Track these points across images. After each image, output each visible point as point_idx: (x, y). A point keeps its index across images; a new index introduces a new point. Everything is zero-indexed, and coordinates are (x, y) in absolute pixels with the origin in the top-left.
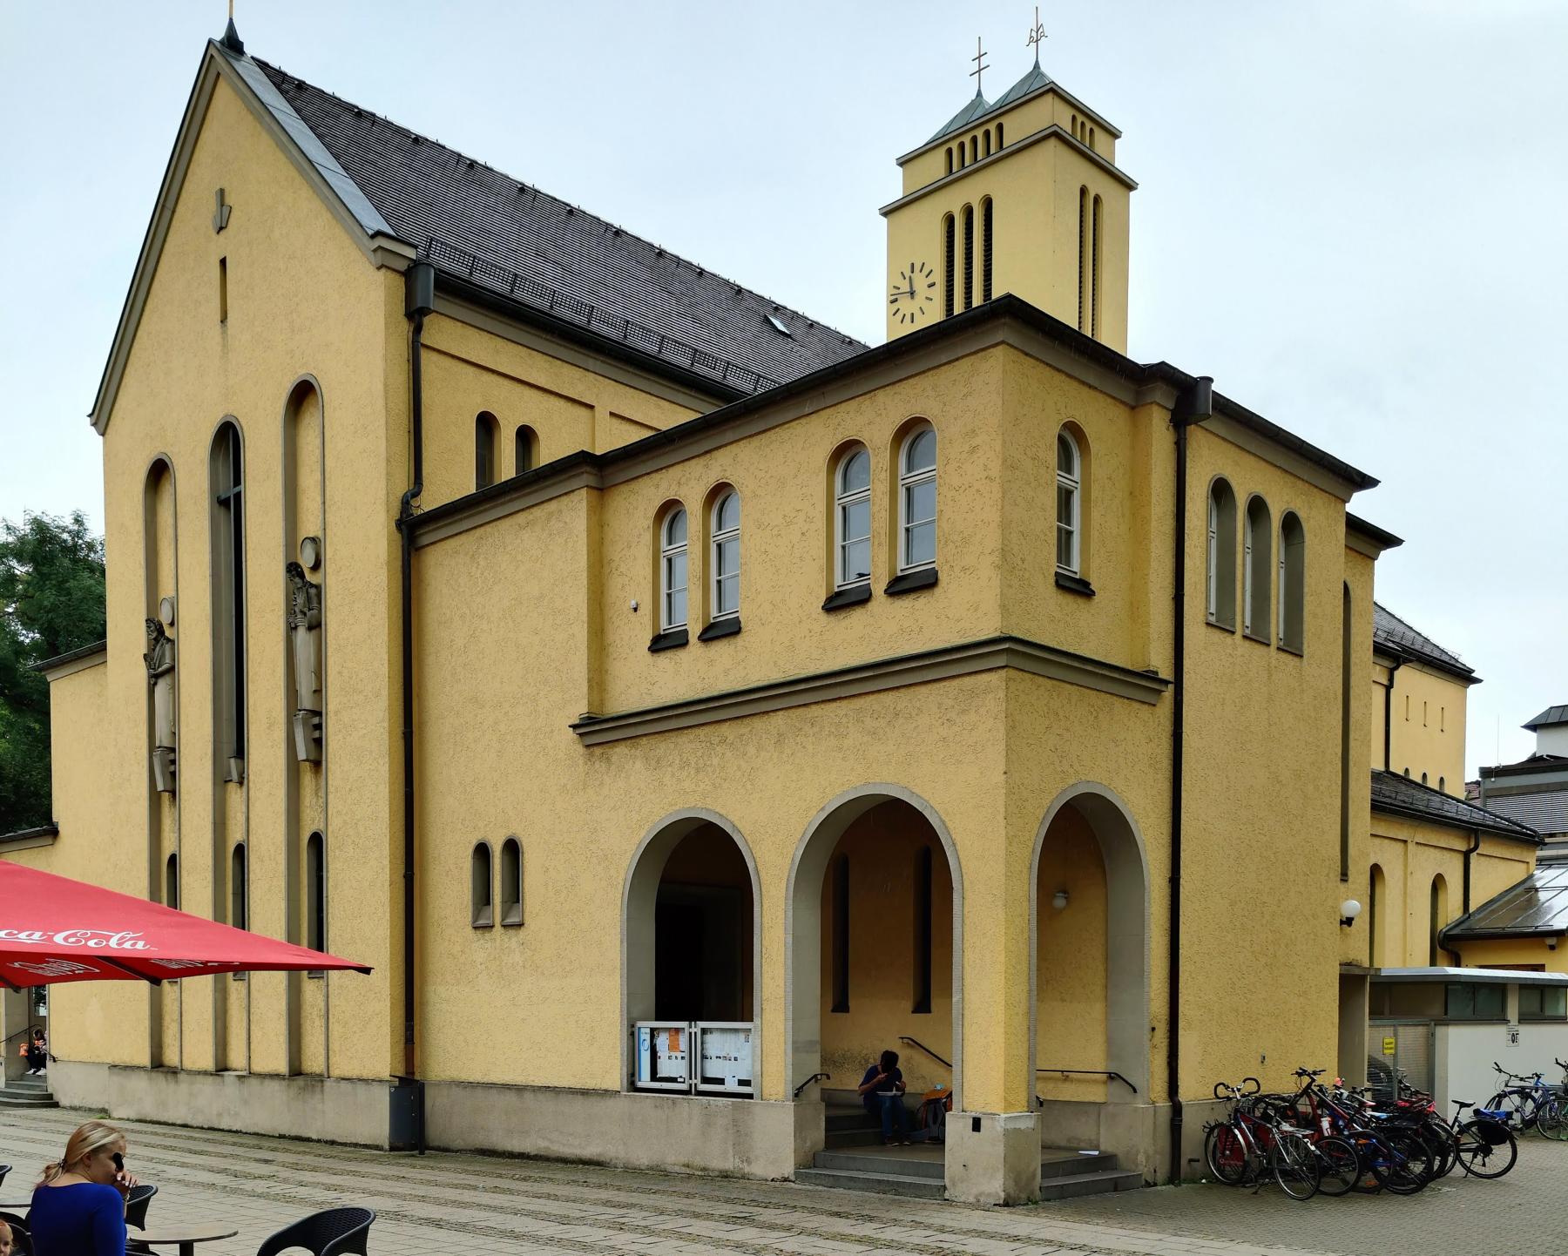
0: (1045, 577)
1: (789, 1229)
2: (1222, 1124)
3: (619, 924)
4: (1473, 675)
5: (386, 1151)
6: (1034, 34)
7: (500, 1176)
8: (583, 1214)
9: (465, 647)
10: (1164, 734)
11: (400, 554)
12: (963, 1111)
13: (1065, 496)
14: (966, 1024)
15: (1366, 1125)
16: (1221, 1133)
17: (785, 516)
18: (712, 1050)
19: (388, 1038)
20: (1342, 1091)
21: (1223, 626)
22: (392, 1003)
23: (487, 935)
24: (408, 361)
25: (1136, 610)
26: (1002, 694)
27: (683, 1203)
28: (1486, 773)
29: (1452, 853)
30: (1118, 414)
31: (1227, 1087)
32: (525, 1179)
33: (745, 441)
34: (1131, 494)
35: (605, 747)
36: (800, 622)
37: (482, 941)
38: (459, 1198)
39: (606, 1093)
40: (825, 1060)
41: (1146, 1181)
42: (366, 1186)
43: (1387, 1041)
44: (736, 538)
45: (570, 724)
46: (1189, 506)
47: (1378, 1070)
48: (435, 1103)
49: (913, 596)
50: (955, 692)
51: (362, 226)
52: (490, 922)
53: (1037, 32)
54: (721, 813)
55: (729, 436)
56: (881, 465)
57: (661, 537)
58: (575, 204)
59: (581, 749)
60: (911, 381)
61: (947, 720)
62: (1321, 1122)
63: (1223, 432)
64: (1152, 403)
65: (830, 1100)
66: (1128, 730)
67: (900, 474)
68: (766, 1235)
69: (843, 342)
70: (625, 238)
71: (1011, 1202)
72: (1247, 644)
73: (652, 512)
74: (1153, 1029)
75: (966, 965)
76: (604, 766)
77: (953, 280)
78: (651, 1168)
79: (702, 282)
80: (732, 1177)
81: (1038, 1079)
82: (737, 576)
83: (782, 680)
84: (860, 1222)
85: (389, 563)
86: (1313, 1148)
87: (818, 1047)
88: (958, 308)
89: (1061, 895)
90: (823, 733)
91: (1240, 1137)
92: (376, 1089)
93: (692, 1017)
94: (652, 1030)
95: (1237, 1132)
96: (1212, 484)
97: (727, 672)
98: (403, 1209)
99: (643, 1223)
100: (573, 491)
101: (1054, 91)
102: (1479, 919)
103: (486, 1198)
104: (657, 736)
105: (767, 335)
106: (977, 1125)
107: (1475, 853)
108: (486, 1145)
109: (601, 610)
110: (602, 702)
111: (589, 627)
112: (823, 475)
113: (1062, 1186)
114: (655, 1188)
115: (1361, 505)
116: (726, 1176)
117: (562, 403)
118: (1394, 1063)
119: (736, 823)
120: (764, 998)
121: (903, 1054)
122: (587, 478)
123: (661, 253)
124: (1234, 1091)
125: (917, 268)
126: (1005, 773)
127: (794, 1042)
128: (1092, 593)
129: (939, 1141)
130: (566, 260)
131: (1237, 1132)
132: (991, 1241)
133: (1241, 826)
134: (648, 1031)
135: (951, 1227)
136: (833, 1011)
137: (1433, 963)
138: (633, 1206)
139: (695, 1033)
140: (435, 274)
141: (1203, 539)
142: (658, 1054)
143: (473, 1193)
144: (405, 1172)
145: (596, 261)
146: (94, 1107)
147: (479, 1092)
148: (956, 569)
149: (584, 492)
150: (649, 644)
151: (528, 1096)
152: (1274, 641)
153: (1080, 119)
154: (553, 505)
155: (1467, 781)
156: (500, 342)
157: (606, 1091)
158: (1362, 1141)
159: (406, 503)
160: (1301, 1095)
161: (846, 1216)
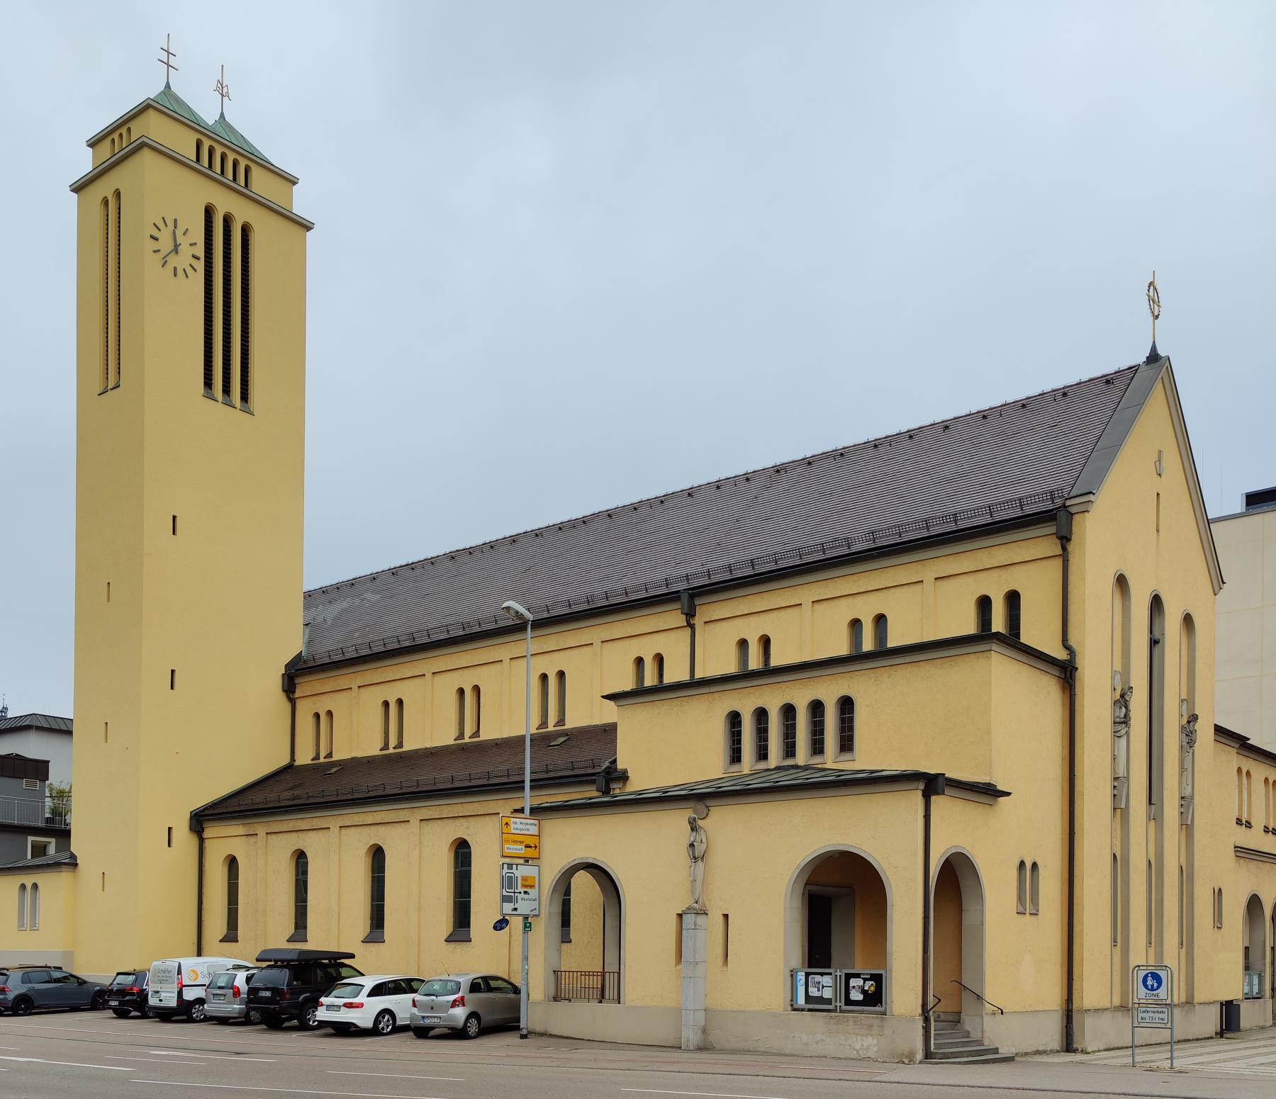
4: (1248, 742)
146: (1030, 1051)
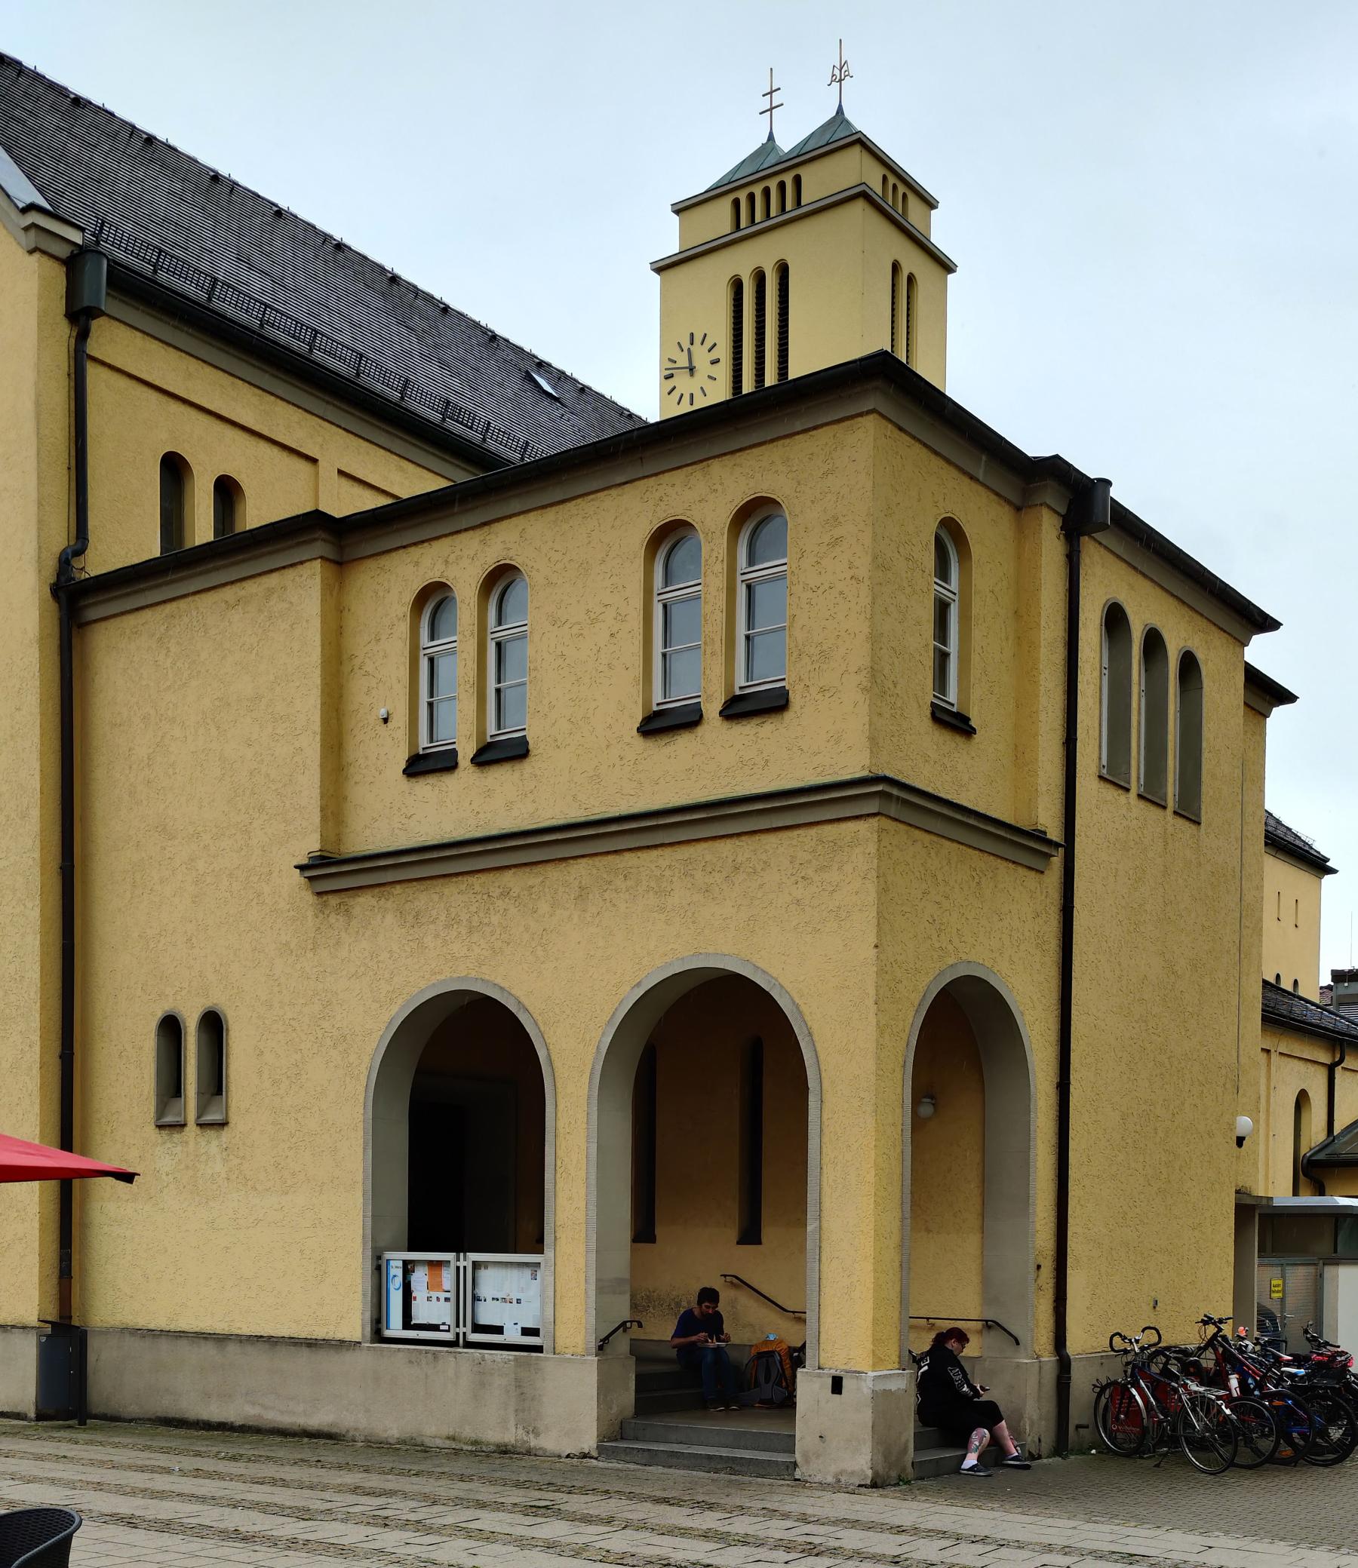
0: (920, 706)
1: (610, 1521)
2: (1115, 1383)
3: (361, 1126)
4: (1327, 864)
5: (31, 1420)
6: (837, 72)
7: (198, 1454)
8: (328, 1506)
9: (149, 759)
10: (1053, 908)
11: (56, 630)
12: (819, 1368)
13: (942, 608)
14: (824, 1259)
15: (1279, 1381)
16: (1113, 1394)
17: (588, 611)
18: (486, 1290)
19: (36, 1270)
20: (1247, 1342)
21: (1117, 782)
22: (41, 1224)
23: (176, 1137)
24: (69, 375)
25: (1021, 755)
26: (872, 848)
27: (459, 1489)
28: (1338, 976)
29: (1316, 1066)
30: (1002, 514)
31: (1124, 1338)
32: (234, 1458)
33: (536, 513)
34: (1016, 612)
35: (343, 895)
36: (608, 746)
37: (169, 1145)
38: (149, 1485)
39: (342, 1345)
40: (634, 1306)
41: (1030, 1452)
42: (14, 1469)
43: (1274, 1282)
44: (452, 652)
45: (296, 863)
46: (1082, 634)
47: (1267, 1320)
48: (101, 1357)
49: (756, 721)
50: (813, 843)
51: (8, 196)
52: (181, 1119)
53: (841, 71)
54: (502, 985)
55: (515, 505)
56: (715, 554)
57: (489, 614)
58: (283, 205)
59: (309, 897)
60: (756, 451)
61: (803, 878)
62: (1228, 1380)
63: (1120, 551)
64: (1041, 505)
65: (641, 1353)
66: (1013, 900)
67: (655, 589)
68: (581, 1530)
69: (621, 414)
70: (349, 255)
71: (879, 1482)
72: (1142, 804)
73: (410, 597)
74: (1039, 1267)
75: (824, 1184)
76: (341, 920)
77: (741, 358)
78: (404, 1442)
79: (447, 321)
80: (513, 1453)
81: (912, 1327)
82: (523, 684)
83: (583, 819)
84: (696, 1510)
85: (41, 640)
86: (1228, 1412)
87: (627, 1288)
88: (748, 386)
89: (928, 1100)
90: (639, 888)
91: (1138, 1398)
92: (17, 1337)
93: (459, 1247)
94: (405, 1263)
95: (1134, 1391)
96: (1106, 609)
97: (509, 806)
98: (74, 1502)
99: (413, 1517)
100: (302, 563)
101: (862, 142)
102: (1346, 1143)
103: (188, 1485)
104: (415, 883)
105: (529, 398)
106: (837, 1385)
107: (1340, 1067)
108: (173, 1412)
109: (338, 719)
110: (339, 839)
111: (323, 740)
112: (640, 562)
113: (937, 1461)
114: (416, 1468)
115: (1261, 652)
116: (504, 1451)
117: (275, 451)
118: (1282, 1308)
119: (523, 999)
120: (558, 1223)
121: (726, 1295)
122: (320, 548)
123: (394, 279)
124: (1131, 1343)
125: (698, 339)
126: (876, 946)
127: (597, 1280)
128: (973, 731)
129: (787, 1404)
130: (276, 271)
131: (1134, 1391)
132: (870, 1534)
133: (1134, 1024)
134: (400, 1264)
135: (814, 1516)
136: (738, 1243)
137: (1295, 1193)
138: (391, 1493)
139: (465, 1267)
140: (108, 265)
141: (1096, 674)
142: (413, 1295)
143: (166, 1478)
144: (64, 1449)
145: (313, 277)
147: (164, 1344)
148: (812, 689)
149: (317, 564)
150: (403, 766)
151: (232, 1348)
152: (1171, 804)
153: (892, 180)
154: (273, 580)
155: (1321, 985)
156: (194, 365)
157: (342, 1342)
158: (1276, 1403)
159: (65, 562)
160: (1205, 1348)
161: (677, 1503)
